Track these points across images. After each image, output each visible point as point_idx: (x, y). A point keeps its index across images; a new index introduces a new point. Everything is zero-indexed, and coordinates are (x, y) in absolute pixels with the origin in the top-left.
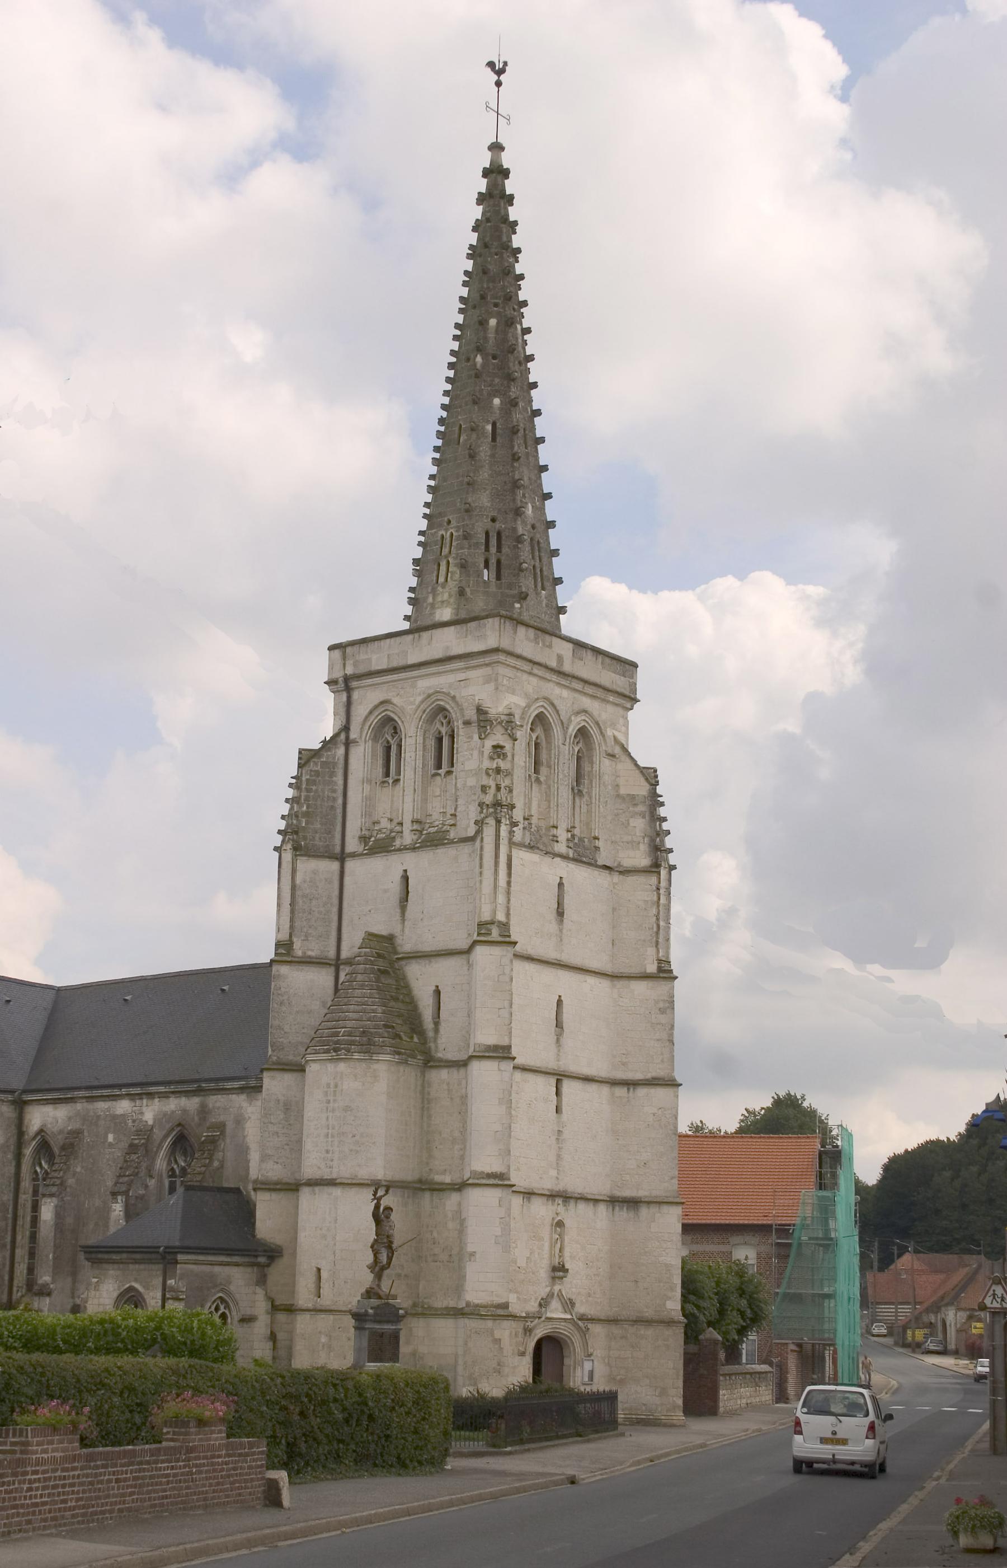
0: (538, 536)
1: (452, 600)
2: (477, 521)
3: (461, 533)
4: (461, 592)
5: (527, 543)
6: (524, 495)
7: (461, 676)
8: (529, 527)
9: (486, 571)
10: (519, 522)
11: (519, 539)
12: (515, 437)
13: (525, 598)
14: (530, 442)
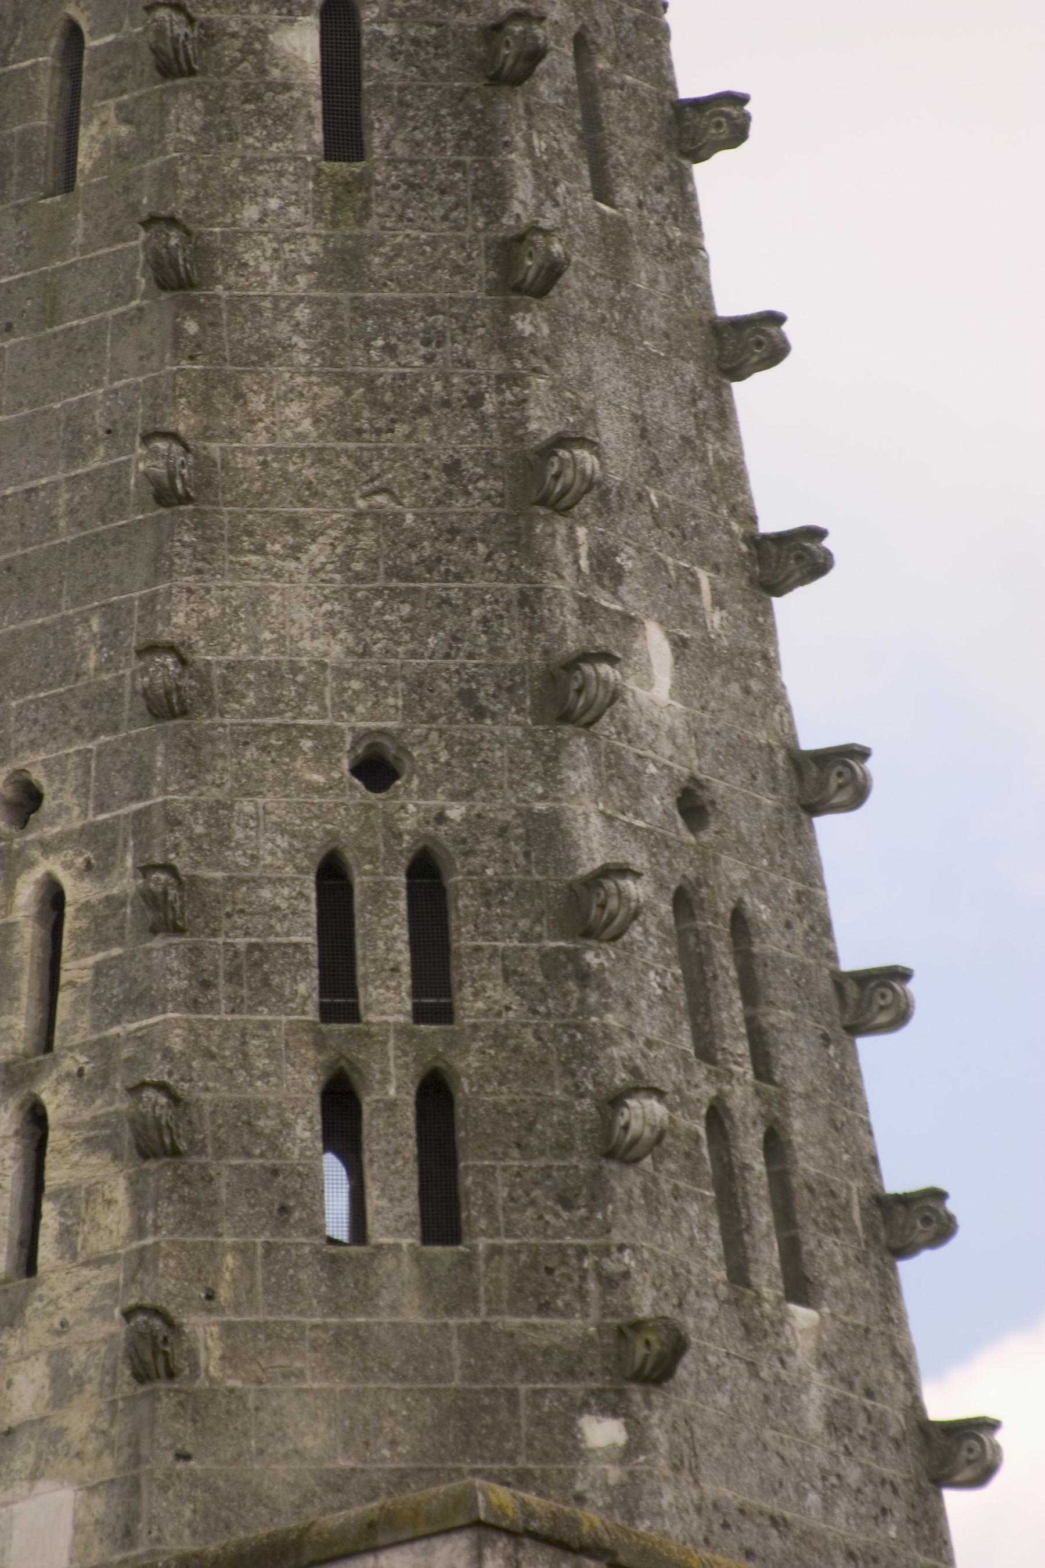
0: (733, 871)
1: (79, 1420)
2: (248, 785)
3: (125, 882)
4: (153, 1353)
5: (650, 941)
6: (606, 567)
7: (412, 1495)
8: (660, 802)
9: (333, 1171)
10: (580, 776)
11: (585, 909)
12: (512, 106)
13: (659, 1373)
14: (630, 143)
